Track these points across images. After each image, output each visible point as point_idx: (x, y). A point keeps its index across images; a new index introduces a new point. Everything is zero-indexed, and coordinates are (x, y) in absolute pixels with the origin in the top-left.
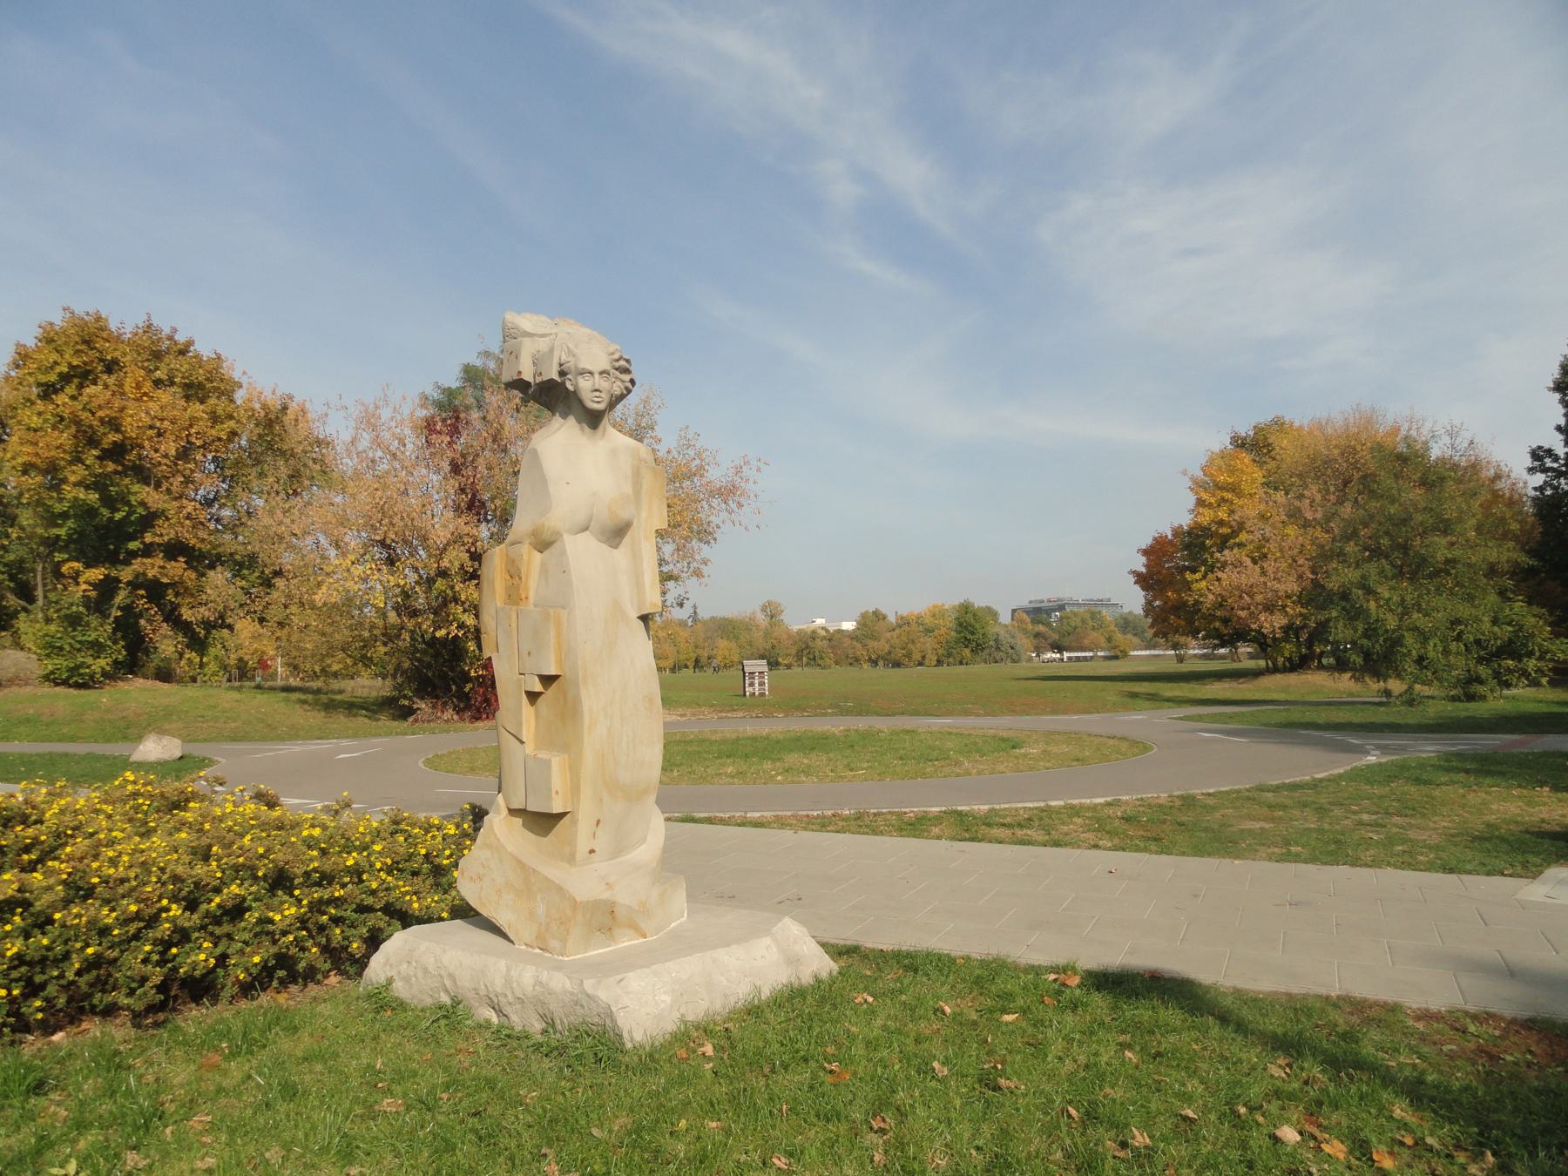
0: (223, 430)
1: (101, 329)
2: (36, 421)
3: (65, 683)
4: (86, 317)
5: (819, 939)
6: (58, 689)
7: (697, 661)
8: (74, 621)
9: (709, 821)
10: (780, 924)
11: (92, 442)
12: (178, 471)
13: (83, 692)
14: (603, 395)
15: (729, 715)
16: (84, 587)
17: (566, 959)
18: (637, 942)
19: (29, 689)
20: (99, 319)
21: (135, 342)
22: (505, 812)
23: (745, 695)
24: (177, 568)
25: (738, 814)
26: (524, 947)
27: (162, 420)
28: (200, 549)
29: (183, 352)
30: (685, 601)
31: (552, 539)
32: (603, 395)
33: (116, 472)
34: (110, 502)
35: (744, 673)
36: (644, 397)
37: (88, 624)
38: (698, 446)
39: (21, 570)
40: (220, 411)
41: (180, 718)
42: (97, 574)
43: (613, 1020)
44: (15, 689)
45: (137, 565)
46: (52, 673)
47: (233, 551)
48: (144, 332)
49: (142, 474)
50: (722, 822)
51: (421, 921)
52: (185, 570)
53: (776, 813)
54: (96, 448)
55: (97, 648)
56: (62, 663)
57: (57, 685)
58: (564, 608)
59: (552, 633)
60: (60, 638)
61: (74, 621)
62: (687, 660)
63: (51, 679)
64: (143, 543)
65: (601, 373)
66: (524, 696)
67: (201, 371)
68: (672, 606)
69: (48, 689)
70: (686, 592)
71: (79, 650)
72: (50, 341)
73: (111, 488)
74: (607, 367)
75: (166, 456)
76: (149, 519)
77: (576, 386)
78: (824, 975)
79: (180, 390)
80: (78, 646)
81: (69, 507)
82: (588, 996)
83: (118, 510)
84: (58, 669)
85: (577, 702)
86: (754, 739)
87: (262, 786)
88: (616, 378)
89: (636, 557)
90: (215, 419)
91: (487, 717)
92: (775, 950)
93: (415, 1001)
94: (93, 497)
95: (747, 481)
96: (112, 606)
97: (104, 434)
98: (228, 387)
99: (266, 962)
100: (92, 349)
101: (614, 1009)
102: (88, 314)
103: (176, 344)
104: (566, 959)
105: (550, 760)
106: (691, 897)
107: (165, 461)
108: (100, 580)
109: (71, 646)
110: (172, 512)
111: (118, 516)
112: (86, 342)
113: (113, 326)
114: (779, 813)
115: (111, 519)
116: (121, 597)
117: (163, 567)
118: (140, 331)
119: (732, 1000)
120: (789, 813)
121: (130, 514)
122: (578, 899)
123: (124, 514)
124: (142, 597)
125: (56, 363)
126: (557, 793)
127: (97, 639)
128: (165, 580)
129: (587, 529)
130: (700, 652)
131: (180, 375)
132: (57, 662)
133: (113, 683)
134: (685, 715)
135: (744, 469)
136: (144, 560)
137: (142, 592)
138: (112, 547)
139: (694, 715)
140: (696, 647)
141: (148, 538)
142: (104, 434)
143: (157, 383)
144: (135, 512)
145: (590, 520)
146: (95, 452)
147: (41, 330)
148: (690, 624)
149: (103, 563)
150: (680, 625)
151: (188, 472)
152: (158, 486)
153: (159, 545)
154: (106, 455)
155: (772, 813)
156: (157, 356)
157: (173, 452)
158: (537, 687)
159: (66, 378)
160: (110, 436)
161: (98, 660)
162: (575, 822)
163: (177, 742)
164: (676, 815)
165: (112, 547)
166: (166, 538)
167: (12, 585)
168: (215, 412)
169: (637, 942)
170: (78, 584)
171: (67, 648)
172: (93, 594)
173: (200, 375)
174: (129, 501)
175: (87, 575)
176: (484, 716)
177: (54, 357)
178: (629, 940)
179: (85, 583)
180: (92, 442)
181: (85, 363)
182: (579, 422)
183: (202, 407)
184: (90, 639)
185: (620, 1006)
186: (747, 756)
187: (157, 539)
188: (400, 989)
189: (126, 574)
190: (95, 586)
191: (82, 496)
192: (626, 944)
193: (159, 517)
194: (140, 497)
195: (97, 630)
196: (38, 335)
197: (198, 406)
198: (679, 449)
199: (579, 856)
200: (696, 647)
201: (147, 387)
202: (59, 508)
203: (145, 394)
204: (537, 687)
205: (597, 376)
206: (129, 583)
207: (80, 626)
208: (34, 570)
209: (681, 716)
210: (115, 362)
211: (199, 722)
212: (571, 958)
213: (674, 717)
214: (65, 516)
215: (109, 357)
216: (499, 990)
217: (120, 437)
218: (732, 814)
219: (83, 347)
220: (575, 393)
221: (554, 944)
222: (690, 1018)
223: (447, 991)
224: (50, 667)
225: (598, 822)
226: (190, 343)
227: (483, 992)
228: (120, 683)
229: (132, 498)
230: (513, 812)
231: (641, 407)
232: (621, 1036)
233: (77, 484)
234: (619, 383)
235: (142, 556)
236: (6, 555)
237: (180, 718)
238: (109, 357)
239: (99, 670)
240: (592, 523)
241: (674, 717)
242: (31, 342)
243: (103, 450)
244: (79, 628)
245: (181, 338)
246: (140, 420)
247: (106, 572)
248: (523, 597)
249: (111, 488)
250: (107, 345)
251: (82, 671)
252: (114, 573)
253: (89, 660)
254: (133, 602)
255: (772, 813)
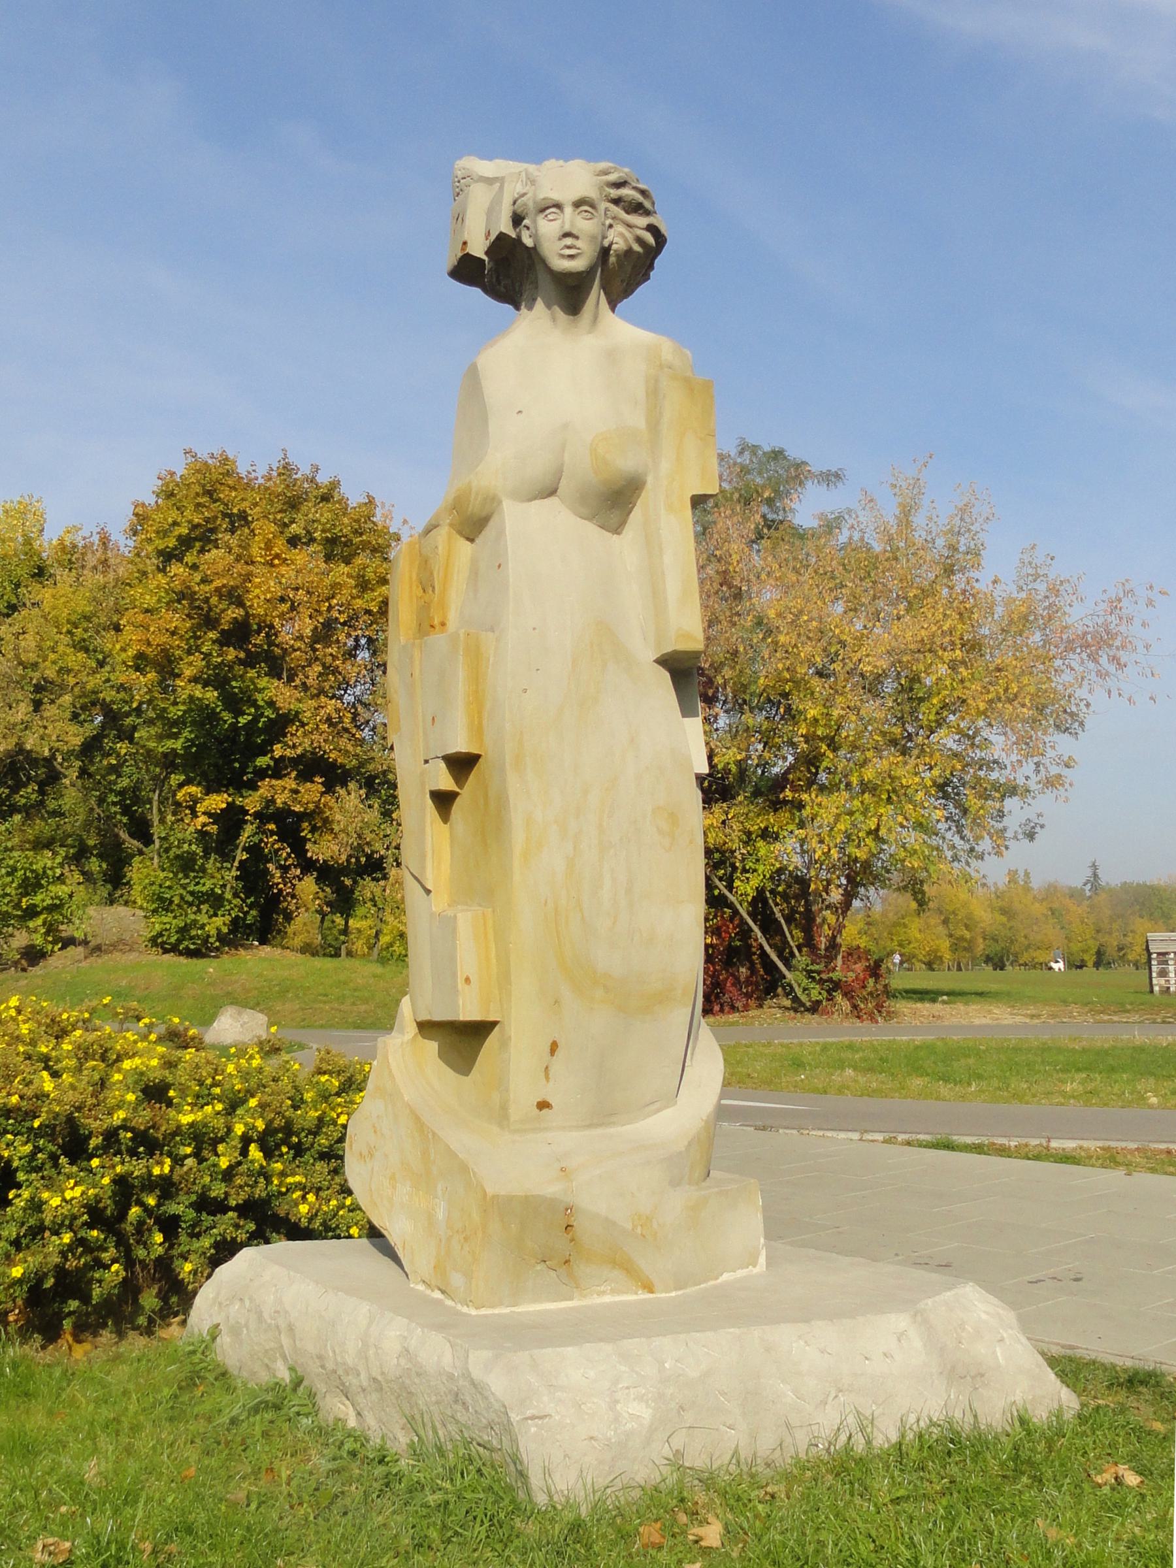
0: (373, 600)
1: (228, 474)
2: (149, 601)
3: (174, 949)
4: (210, 461)
5: (1045, 1347)
6: (166, 956)
7: (1099, 954)
8: (186, 864)
9: (978, 1149)
10: (948, 1295)
11: (210, 622)
12: (317, 659)
13: (195, 961)
14: (579, 243)
15: (1115, 1018)
16: (203, 819)
17: (473, 1312)
18: (634, 1297)
19: (133, 956)
20: (225, 460)
21: (267, 489)
22: (412, 1030)
23: (1152, 991)
24: (312, 791)
25: (1034, 1142)
26: (421, 1287)
27: (297, 589)
28: (342, 766)
29: (326, 498)
30: (1038, 829)
31: (484, 514)
32: (579, 243)
33: (241, 662)
34: (234, 703)
35: (1150, 954)
36: (960, 505)
37: (203, 870)
38: (1052, 576)
39: (137, 800)
40: (370, 575)
41: (297, 996)
42: (218, 801)
43: (514, 1441)
44: (117, 955)
45: (265, 788)
46: (160, 935)
47: (385, 767)
48: (279, 475)
49: (276, 666)
50: (1003, 1151)
51: (297, 1232)
52: (322, 794)
53: (1107, 1144)
54: (214, 628)
55: (215, 901)
56: (169, 922)
57: (166, 951)
58: (492, 630)
59: (461, 674)
60: (170, 888)
61: (186, 864)
62: (1084, 951)
63: (157, 942)
64: (272, 758)
65: (578, 204)
66: (429, 802)
67: (346, 521)
68: (1016, 838)
69: (155, 957)
70: (1039, 815)
71: (191, 904)
72: (171, 495)
73: (234, 684)
74: (592, 194)
75: (300, 638)
76: (281, 724)
77: (535, 236)
78: (1040, 1416)
79: (320, 548)
80: (190, 899)
81: (185, 712)
82: (473, 1383)
83: (244, 713)
84: (166, 930)
85: (502, 802)
86: (1141, 1049)
87: (176, 1020)
88: (614, 218)
89: (651, 545)
90: (364, 585)
91: (722, 1010)
92: (918, 1344)
93: (245, 1374)
94: (211, 695)
95: (1130, 620)
96: (237, 847)
97: (223, 611)
98: (380, 541)
99: (40, 1278)
100: (215, 501)
101: (514, 1417)
102: (212, 456)
103: (318, 487)
104: (473, 1312)
105: (455, 916)
106: (775, 1229)
107: (298, 644)
108: (222, 810)
109: (182, 897)
110: (308, 714)
111: (243, 720)
112: (209, 493)
113: (242, 470)
114: (1113, 1144)
115: (234, 726)
116: (248, 832)
117: (296, 792)
118: (275, 474)
119: (802, 1439)
120: (1133, 1146)
121: (256, 720)
122: (490, 1191)
123: (250, 718)
124: (272, 833)
125: (175, 524)
126: (467, 980)
127: (212, 890)
128: (297, 808)
129: (552, 492)
130: (1104, 939)
131: (320, 527)
132: (165, 920)
133: (233, 951)
134: (1038, 1016)
135: (1125, 603)
136: (274, 782)
137: (272, 827)
138: (237, 765)
139: (1053, 1016)
140: (1098, 931)
141: (278, 750)
142: (223, 611)
143: (293, 541)
144: (262, 715)
145: (559, 474)
146: (212, 635)
147: (160, 482)
148: (1088, 894)
149: (227, 786)
150: (1071, 896)
151: (329, 659)
152: (291, 679)
153: (291, 759)
154: (226, 639)
155: (1100, 1144)
156: (293, 504)
157: (308, 632)
158: (445, 781)
159: (186, 542)
160: (229, 612)
161: (214, 919)
162: (504, 1043)
163: (262, 1018)
164: (921, 1137)
165: (237, 765)
166: (299, 751)
167: (125, 820)
168: (363, 576)
169: (634, 1297)
170: (194, 814)
171: (176, 900)
172: (213, 829)
173: (345, 527)
174: (256, 700)
175: (206, 803)
176: (717, 1008)
177: (173, 515)
178: (614, 1291)
179: (204, 813)
180: (210, 622)
181: (207, 520)
182: (549, 306)
183: (346, 569)
184: (204, 889)
185: (529, 1413)
186: (1113, 1069)
187: (289, 753)
188: (228, 1352)
189: (252, 802)
190: (215, 817)
191: (198, 694)
192: (607, 1299)
193: (292, 722)
194: (267, 695)
195: (213, 877)
196: (155, 489)
197: (344, 569)
198: (1021, 583)
199: (514, 1113)
200: (1098, 931)
201: (280, 546)
202: (175, 712)
203: (277, 556)
204: (445, 781)
205: (568, 210)
206: (257, 815)
207: (193, 871)
208: (150, 801)
209: (1032, 1016)
210: (243, 516)
211: (321, 1002)
212: (483, 1311)
213: (1018, 1019)
214: (179, 723)
215: (235, 511)
216: (350, 1361)
217: (242, 612)
218: (1024, 1141)
219: (204, 500)
220: (535, 248)
221: (457, 1280)
222: (696, 1459)
223: (284, 1358)
224: (158, 927)
225: (554, 1048)
226: (335, 485)
227: (330, 1365)
228: (242, 952)
229: (259, 696)
230: (427, 1028)
231: (957, 521)
232: (522, 1475)
233: (195, 680)
234: (620, 228)
235: (271, 777)
236: (119, 780)
237: (297, 996)
238: (235, 511)
239: (213, 932)
240: (563, 482)
241: (1018, 1019)
242: (150, 500)
243: (223, 632)
244: (192, 874)
245: (323, 479)
246: (268, 590)
247: (230, 799)
248: (436, 622)
249: (234, 684)
250: (233, 494)
251: (193, 933)
252: (239, 801)
253: (203, 918)
254: (261, 841)
255: (1100, 1144)
